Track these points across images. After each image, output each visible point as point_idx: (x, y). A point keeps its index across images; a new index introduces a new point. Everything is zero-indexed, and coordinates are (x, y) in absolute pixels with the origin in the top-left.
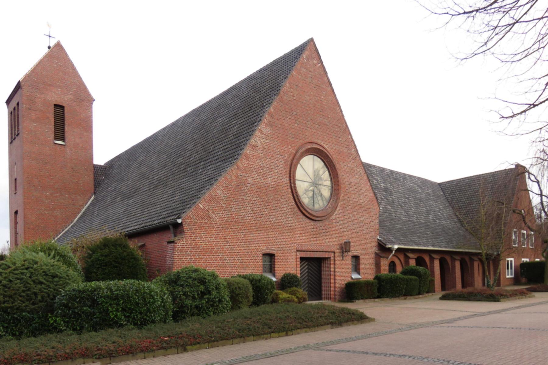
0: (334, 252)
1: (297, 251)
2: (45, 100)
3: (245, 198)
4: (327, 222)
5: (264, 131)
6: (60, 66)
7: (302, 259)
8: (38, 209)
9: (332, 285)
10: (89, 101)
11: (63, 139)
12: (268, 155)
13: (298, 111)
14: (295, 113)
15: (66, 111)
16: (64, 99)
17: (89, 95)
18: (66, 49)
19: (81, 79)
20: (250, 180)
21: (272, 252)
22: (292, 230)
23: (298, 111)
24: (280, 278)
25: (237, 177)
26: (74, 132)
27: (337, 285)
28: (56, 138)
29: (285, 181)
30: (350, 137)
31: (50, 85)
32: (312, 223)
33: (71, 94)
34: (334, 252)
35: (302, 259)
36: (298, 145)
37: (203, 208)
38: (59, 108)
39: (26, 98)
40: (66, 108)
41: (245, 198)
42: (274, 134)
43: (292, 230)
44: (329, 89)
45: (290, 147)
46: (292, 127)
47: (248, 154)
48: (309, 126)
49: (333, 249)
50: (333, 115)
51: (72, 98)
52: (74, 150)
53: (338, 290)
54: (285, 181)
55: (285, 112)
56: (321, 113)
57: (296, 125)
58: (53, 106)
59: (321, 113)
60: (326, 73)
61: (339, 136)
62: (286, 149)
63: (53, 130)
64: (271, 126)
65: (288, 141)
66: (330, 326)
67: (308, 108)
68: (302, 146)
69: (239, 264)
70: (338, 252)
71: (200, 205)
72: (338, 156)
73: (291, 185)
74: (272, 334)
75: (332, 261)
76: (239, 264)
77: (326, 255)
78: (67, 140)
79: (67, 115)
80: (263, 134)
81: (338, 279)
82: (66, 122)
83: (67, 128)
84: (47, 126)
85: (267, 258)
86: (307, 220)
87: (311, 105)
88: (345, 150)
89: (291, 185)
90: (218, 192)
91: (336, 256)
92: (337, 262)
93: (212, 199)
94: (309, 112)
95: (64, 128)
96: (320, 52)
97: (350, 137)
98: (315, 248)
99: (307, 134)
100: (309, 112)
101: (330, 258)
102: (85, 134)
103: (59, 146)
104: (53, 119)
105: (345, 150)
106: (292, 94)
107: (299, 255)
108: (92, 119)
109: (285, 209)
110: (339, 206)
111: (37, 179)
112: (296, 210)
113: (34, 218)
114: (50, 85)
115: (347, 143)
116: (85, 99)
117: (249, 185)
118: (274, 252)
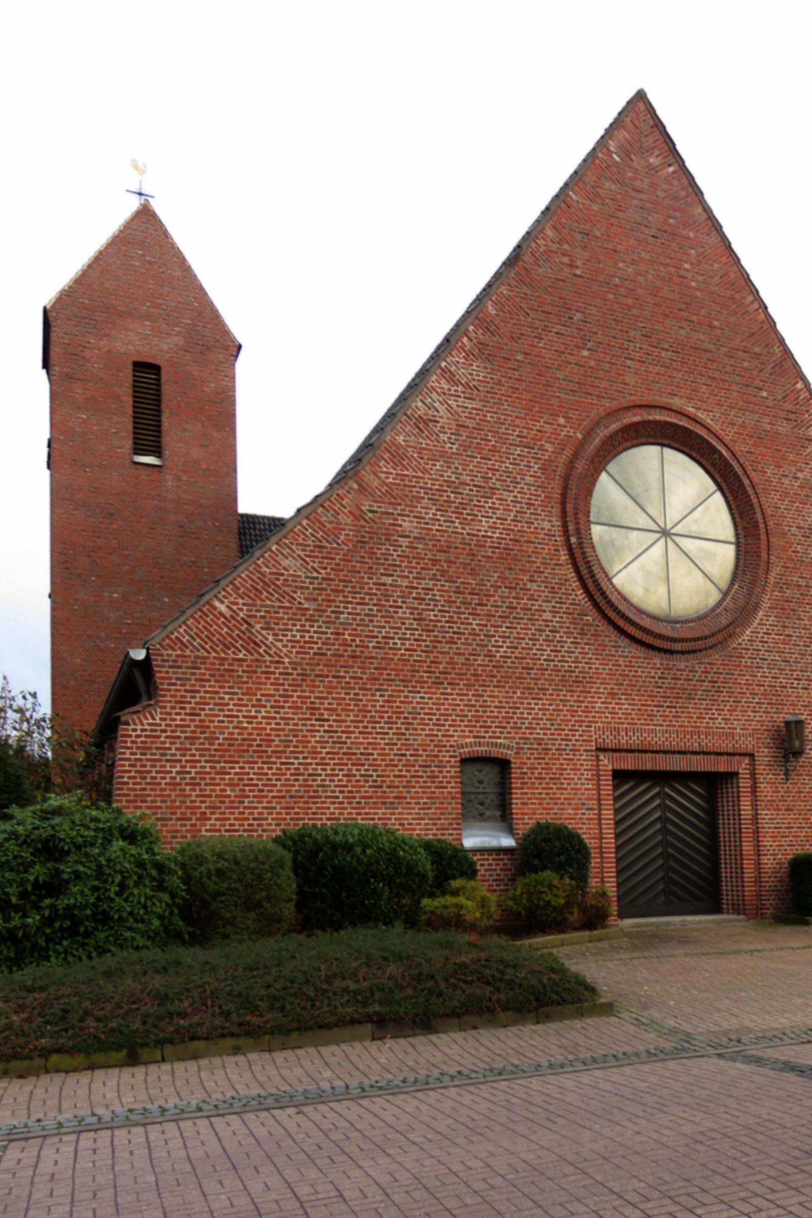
0: (752, 756)
1: (599, 749)
2: (109, 351)
3: (384, 579)
4: (716, 657)
5: (462, 374)
6: (150, 263)
7: (619, 776)
8: (90, 636)
9: (749, 865)
10: (226, 348)
11: (157, 451)
12: (478, 447)
13: (593, 310)
14: (579, 316)
15: (164, 377)
16: (160, 348)
17: (226, 332)
18: (164, 220)
19: (206, 294)
20: (406, 525)
21: (496, 752)
22: (574, 682)
23: (593, 310)
24: (526, 837)
25: (358, 516)
26: (185, 430)
27: (768, 862)
28: (138, 451)
29: (547, 526)
30: (800, 385)
31: (121, 314)
32: (658, 660)
33: (178, 334)
34: (752, 756)
35: (619, 776)
36: (594, 413)
37: (227, 613)
38: (147, 374)
39: (60, 351)
40: (164, 372)
41: (389, 580)
42: (499, 383)
43: (574, 682)
44: (714, 240)
45: (562, 421)
46: (572, 359)
47: (398, 446)
48: (637, 356)
49: (748, 744)
50: (732, 320)
51: (182, 343)
52: (184, 478)
53: (769, 883)
54: (547, 526)
55: (542, 316)
56: (685, 314)
57: (585, 353)
58: (130, 367)
59: (685, 314)
60: (698, 193)
61: (758, 383)
62: (548, 428)
63: (131, 427)
64: (489, 358)
65: (554, 401)
66: (368, 1028)
67: (630, 301)
68: (612, 414)
69: (367, 790)
70: (764, 755)
71: (217, 604)
72: (755, 445)
73: (568, 540)
74: (54, 1058)
75: (745, 783)
76: (367, 790)
77: (721, 766)
78: (167, 453)
79: (167, 389)
80: (457, 383)
81: (767, 842)
82: (163, 405)
83: (166, 421)
84: (116, 419)
85: (490, 774)
86: (636, 651)
87: (640, 291)
88: (783, 428)
89: (568, 540)
90: (285, 563)
91: (760, 769)
92: (765, 789)
93: (265, 585)
94: (635, 311)
95: (159, 421)
96: (669, 130)
97: (800, 385)
98: (675, 743)
99: (627, 379)
100: (635, 311)
101: (737, 774)
102: (215, 434)
103: (147, 471)
104: (131, 400)
105: (783, 428)
106: (566, 260)
107: (607, 763)
108: (234, 396)
109: (547, 616)
110: (766, 603)
111: (88, 556)
112: (591, 617)
113: (78, 661)
114: (121, 314)
115: (788, 406)
116: (218, 347)
117: (404, 542)
118: (510, 754)
